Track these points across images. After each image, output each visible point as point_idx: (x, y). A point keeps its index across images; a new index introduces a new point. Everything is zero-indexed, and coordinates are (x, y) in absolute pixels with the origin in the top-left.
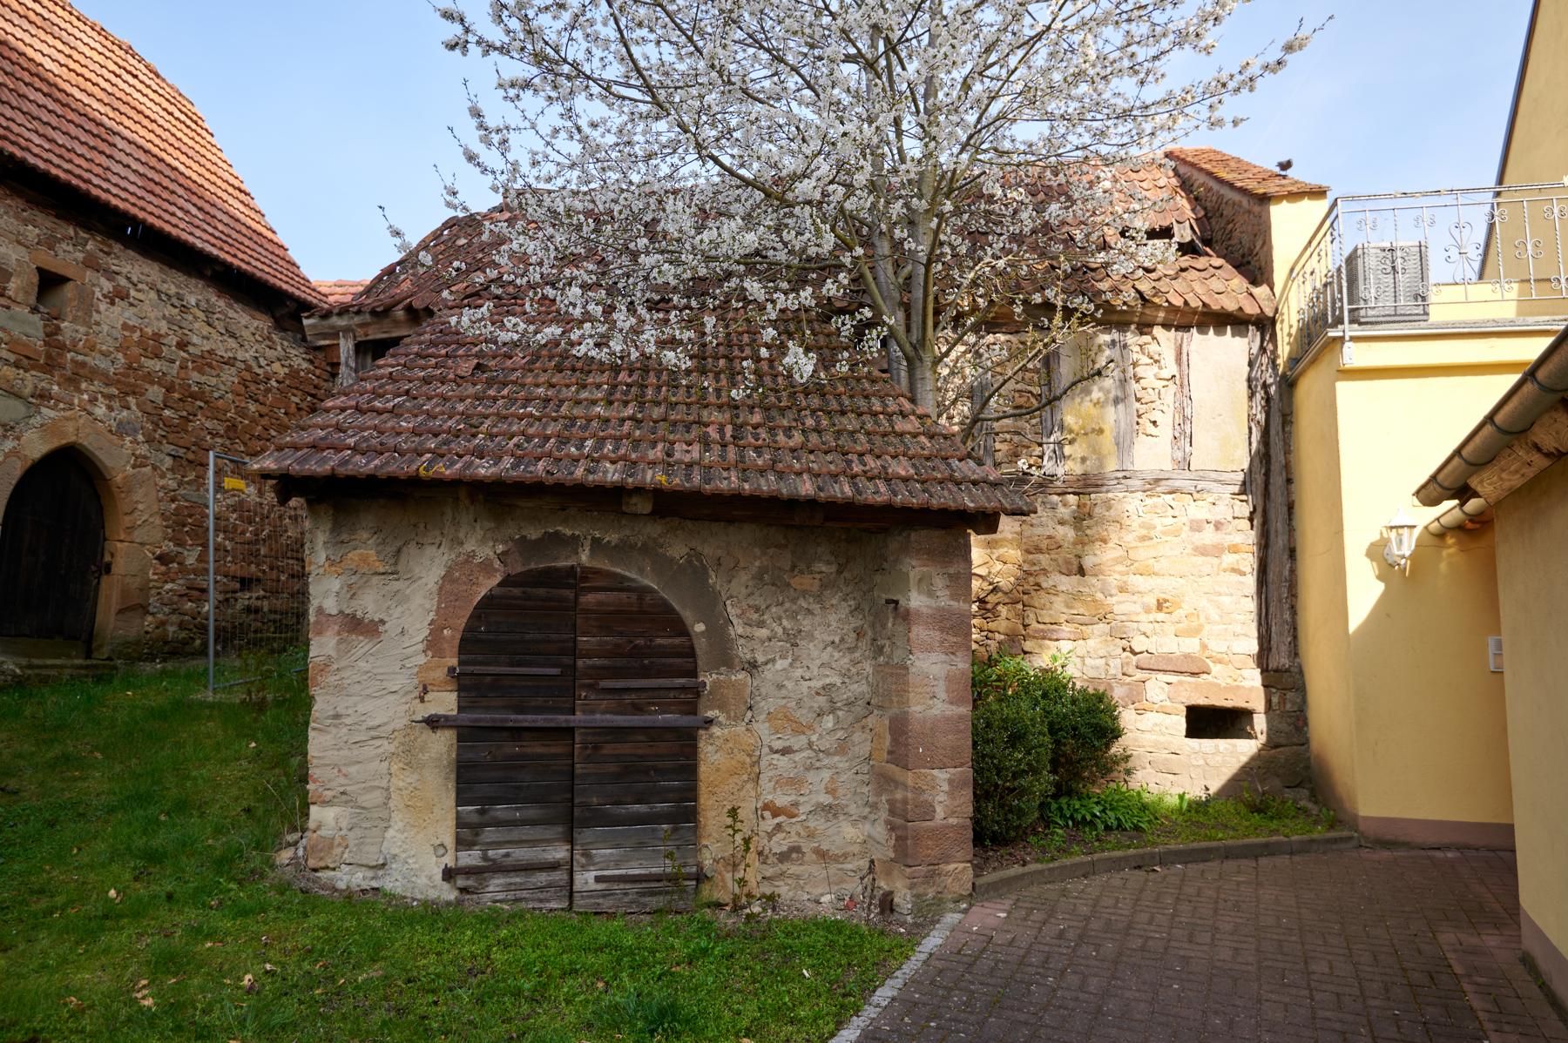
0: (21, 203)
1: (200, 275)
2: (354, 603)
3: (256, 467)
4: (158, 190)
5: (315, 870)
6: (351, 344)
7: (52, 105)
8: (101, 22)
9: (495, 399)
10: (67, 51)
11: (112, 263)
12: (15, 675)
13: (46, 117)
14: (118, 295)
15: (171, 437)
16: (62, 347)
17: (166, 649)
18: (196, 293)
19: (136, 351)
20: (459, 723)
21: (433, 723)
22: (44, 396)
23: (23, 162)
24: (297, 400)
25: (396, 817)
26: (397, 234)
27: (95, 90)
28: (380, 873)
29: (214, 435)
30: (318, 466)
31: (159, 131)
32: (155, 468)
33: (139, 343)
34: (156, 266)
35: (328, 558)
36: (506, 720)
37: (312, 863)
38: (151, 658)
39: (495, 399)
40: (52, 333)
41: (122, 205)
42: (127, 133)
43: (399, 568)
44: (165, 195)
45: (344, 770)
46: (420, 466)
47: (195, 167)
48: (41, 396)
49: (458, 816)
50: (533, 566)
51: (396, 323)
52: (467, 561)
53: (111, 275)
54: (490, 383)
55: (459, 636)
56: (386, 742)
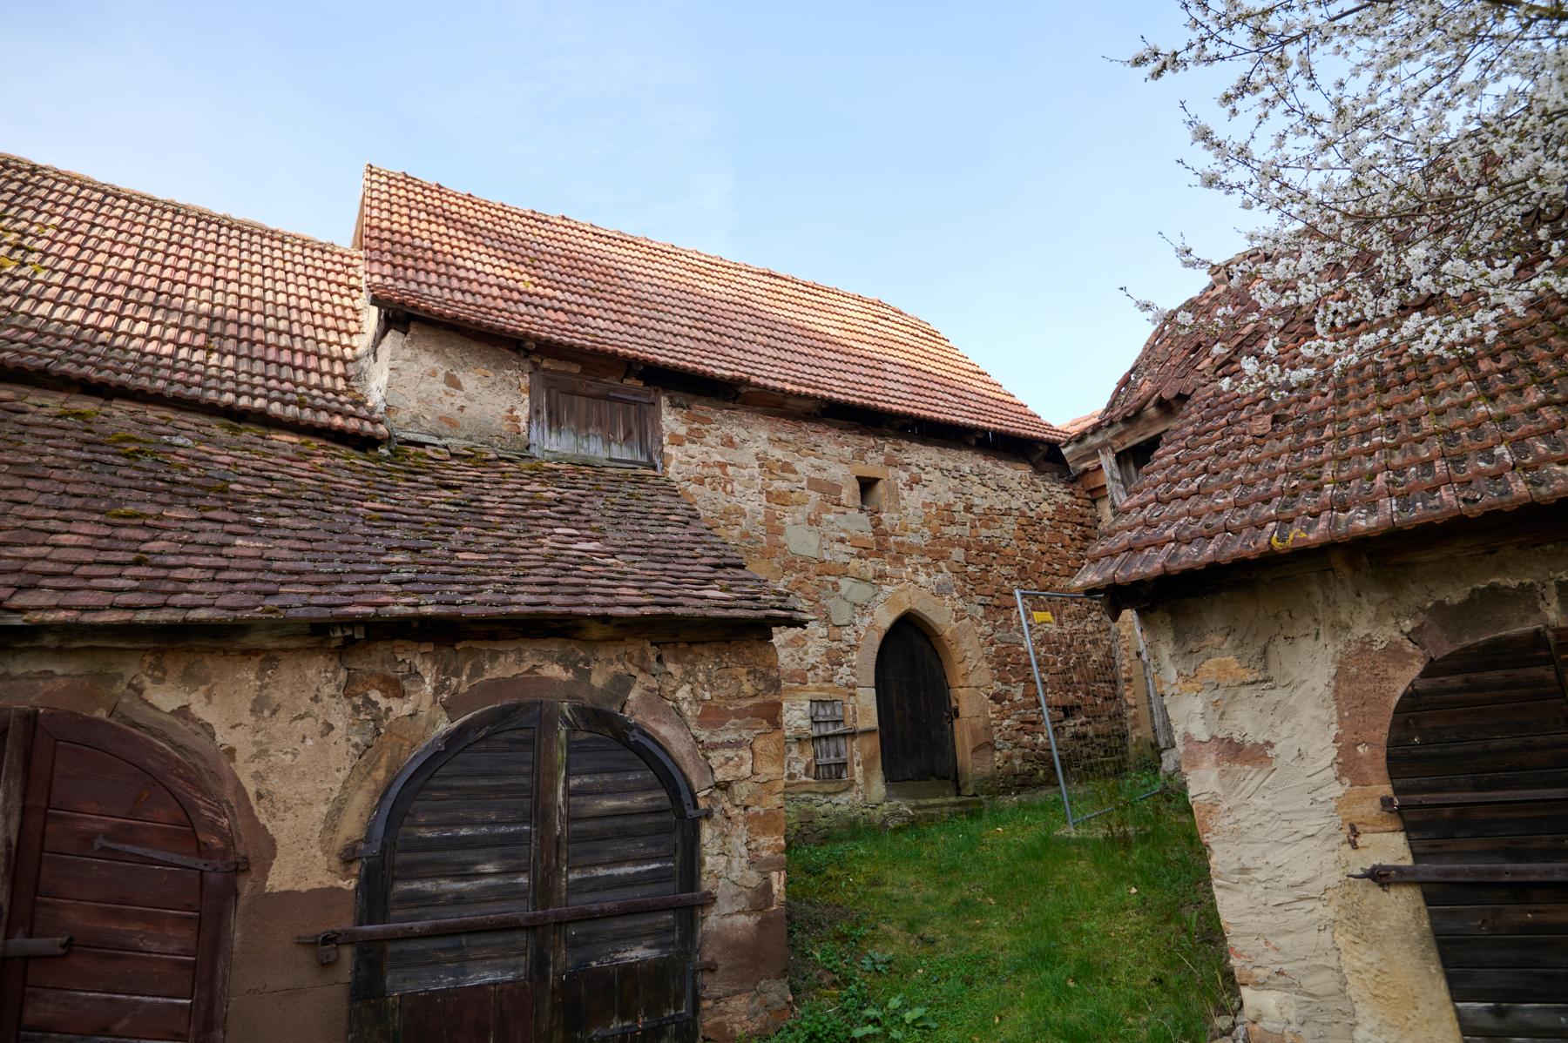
0: (836, 432)
2: (1226, 724)
3: (1079, 583)
4: (922, 391)
6: (1111, 457)
7: (840, 357)
9: (1319, 445)
11: (902, 457)
12: (909, 817)
14: (914, 481)
16: (885, 534)
18: (968, 462)
19: (936, 522)
20: (1421, 877)
21: (1381, 877)
22: (881, 576)
23: (831, 398)
24: (1068, 532)
25: (1363, 1011)
26: (1147, 307)
27: (865, 338)
29: (1010, 580)
30: (1150, 565)
32: (972, 618)
35: (1180, 674)
36: (1499, 872)
38: (1006, 791)
39: (1319, 445)
40: (877, 525)
41: (901, 409)
43: (1271, 673)
46: (1269, 538)
48: (880, 577)
49: (1460, 1016)
50: (1468, 641)
51: (1151, 422)
52: (1362, 651)
53: (905, 466)
54: (1300, 430)
55: (1382, 754)
56: (1319, 905)
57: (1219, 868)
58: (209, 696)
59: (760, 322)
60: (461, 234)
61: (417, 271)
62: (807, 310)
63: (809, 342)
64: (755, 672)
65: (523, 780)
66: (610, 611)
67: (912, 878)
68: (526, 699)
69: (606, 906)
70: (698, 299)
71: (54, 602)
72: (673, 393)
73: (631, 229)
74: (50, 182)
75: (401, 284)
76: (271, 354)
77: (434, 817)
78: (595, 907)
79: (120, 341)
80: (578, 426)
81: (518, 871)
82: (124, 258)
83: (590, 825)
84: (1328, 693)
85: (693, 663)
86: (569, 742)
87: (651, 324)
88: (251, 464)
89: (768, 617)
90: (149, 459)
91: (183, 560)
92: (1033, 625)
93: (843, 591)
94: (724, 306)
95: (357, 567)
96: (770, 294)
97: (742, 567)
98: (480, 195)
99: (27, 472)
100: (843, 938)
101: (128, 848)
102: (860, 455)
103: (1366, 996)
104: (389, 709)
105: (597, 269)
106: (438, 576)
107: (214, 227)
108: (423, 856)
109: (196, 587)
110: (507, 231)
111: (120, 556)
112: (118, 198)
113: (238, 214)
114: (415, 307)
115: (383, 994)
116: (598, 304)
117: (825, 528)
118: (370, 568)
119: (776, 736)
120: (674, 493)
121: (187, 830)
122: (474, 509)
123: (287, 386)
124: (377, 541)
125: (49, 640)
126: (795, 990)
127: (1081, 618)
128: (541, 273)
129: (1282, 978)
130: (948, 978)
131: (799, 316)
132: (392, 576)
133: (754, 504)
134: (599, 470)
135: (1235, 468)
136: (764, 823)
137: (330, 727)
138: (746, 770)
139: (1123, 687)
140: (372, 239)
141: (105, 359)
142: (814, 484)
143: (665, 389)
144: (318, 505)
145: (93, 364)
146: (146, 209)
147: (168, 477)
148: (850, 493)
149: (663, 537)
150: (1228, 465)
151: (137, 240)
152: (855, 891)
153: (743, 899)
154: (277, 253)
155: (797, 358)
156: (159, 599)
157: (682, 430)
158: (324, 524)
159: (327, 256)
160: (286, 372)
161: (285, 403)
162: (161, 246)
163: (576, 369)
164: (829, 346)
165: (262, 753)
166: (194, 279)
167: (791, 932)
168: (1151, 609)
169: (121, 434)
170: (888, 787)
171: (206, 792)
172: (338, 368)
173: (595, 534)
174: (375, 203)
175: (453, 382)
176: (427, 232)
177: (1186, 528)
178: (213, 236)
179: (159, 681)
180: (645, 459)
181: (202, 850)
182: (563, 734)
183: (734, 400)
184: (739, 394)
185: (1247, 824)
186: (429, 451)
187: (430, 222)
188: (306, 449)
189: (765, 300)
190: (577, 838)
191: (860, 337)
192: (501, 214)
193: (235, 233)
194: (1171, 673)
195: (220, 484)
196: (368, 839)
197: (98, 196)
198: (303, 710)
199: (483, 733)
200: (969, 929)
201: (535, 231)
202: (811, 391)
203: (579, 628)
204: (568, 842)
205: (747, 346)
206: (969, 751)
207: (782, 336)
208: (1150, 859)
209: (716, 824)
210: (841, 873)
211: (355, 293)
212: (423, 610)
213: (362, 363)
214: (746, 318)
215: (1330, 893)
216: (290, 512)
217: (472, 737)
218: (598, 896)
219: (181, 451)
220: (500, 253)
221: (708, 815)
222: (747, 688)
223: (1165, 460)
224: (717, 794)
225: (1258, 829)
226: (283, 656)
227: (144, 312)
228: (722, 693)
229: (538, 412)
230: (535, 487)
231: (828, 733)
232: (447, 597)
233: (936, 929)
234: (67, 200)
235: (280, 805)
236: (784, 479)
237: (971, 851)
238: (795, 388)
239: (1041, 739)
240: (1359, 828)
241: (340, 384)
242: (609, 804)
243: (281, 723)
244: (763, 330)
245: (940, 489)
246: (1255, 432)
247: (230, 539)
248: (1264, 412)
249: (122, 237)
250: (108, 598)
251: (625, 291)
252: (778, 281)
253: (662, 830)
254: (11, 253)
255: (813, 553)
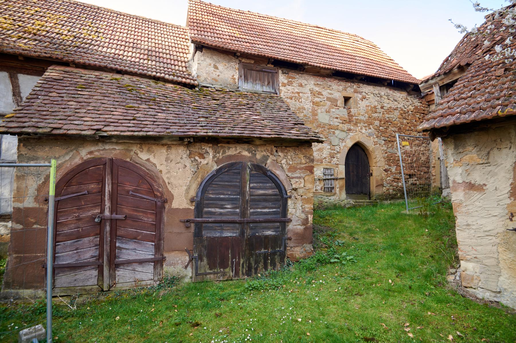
1: (384, 85)
2: (469, 177)
3: (421, 128)
4: (369, 66)
5: (466, 287)
6: (438, 88)
7: (340, 55)
8: (347, 32)
10: (341, 41)
11: (360, 90)
13: (339, 58)
15: (383, 135)
16: (352, 116)
17: (390, 197)
18: (384, 91)
19: (370, 112)
22: (350, 130)
24: (418, 116)
27: (349, 48)
28: (498, 295)
31: (366, 52)
32: (380, 144)
33: (371, 110)
34: (372, 87)
35: (454, 160)
37: (464, 284)
41: (361, 72)
42: (358, 55)
43: (490, 160)
44: (371, 67)
45: (475, 248)
46: (498, 111)
47: (377, 58)
51: (455, 74)
56: (494, 238)
57: (459, 224)
58: (154, 156)
59: (313, 44)
60: (217, 19)
61: (204, 32)
62: (329, 39)
63: (329, 50)
64: (306, 156)
65: (237, 184)
66: (262, 136)
67: (352, 222)
68: (238, 161)
69: (261, 219)
70: (292, 37)
71: (114, 129)
72: (283, 69)
73: (271, 15)
74: (103, 12)
75: (200, 36)
76: (165, 61)
77: (214, 192)
78: (257, 219)
79: (125, 58)
80: (253, 81)
81: (236, 208)
82: (124, 33)
83: (256, 197)
84: (511, 168)
85: (287, 153)
86: (250, 174)
87: (276, 46)
88: (161, 93)
89: (311, 139)
90: (135, 91)
91: (145, 119)
92: (402, 147)
93: (336, 135)
94: (301, 39)
95: (190, 122)
96: (317, 34)
97: (303, 124)
98: (223, 6)
99: (104, 95)
100: (329, 236)
101: (138, 194)
102: (345, 89)
103: (506, 267)
104: (201, 162)
105: (259, 28)
106: (213, 125)
107: (147, 22)
108: (211, 202)
109: (149, 126)
110: (231, 17)
111: (129, 118)
112: (121, 15)
113: (153, 18)
114: (204, 43)
115: (202, 236)
116: (259, 40)
117: (331, 114)
118: (194, 122)
119: (312, 176)
120: (283, 102)
121: (151, 191)
122: (222, 106)
123: (170, 70)
124: (196, 115)
125: (114, 140)
126: (314, 248)
127: (419, 145)
128: (242, 31)
129: (476, 259)
130: (361, 249)
131: (326, 41)
132: (200, 125)
133: (308, 106)
134: (259, 95)
135: (487, 88)
136: (307, 201)
137: (186, 166)
138: (302, 185)
139: (431, 169)
140: (192, 23)
141: (121, 63)
142: (328, 99)
143: (281, 68)
144: (180, 104)
145: (118, 65)
146: (128, 18)
147: (140, 96)
148: (341, 102)
149: (278, 115)
150: (484, 87)
151: (127, 28)
152: (334, 223)
153: (300, 221)
154: (165, 30)
155: (325, 56)
156: (140, 129)
157: (286, 81)
158: (181, 110)
159: (179, 30)
160: (169, 66)
161: (170, 75)
162: (133, 29)
163: (253, 62)
164: (336, 51)
165: (169, 172)
166: (143, 39)
167: (314, 233)
168: (447, 138)
169: (127, 84)
170: (347, 196)
171: (155, 182)
172: (183, 64)
173: (258, 114)
174: (192, 11)
175: (216, 67)
176: (207, 19)
177: (464, 108)
178: (147, 25)
179: (142, 152)
180: (274, 91)
181: (155, 196)
182: (248, 172)
183: (303, 71)
184: (305, 69)
185: (472, 211)
186: (210, 89)
187: (208, 16)
188: (176, 88)
189: (315, 36)
190: (252, 200)
191: (348, 48)
192: (229, 11)
193: (153, 24)
194: (451, 160)
195: (153, 98)
196: (197, 196)
197: (116, 15)
198: (178, 161)
199: (226, 170)
200: (369, 237)
201: (240, 16)
202: (329, 67)
203: (253, 141)
204: (250, 201)
205: (308, 52)
206: (375, 187)
207: (320, 48)
208: (434, 222)
209: (292, 200)
210: (330, 218)
211: (187, 41)
212: (208, 134)
213: (190, 63)
214: (308, 43)
215: (499, 234)
216: (172, 106)
217: (223, 171)
218: (258, 216)
219: (143, 89)
220: (229, 25)
221: (290, 197)
222: (303, 161)
223: (459, 86)
224: (293, 191)
225: (476, 212)
226: (172, 146)
227: (130, 49)
228: (295, 162)
229: (241, 76)
230: (240, 100)
231: (328, 178)
232: (215, 130)
233: (360, 236)
234: (108, 17)
235: (174, 186)
236: (319, 97)
237: (372, 215)
238: (324, 66)
239: (400, 184)
240: (514, 214)
241: (184, 69)
242: (261, 192)
243: (173, 164)
244: (314, 47)
245: (373, 101)
246: (497, 75)
247: (157, 114)
248: (501, 68)
249: (123, 27)
250: (127, 129)
251: (268, 35)
252: (320, 29)
253: (277, 200)
254: (95, 34)
255: (327, 122)
